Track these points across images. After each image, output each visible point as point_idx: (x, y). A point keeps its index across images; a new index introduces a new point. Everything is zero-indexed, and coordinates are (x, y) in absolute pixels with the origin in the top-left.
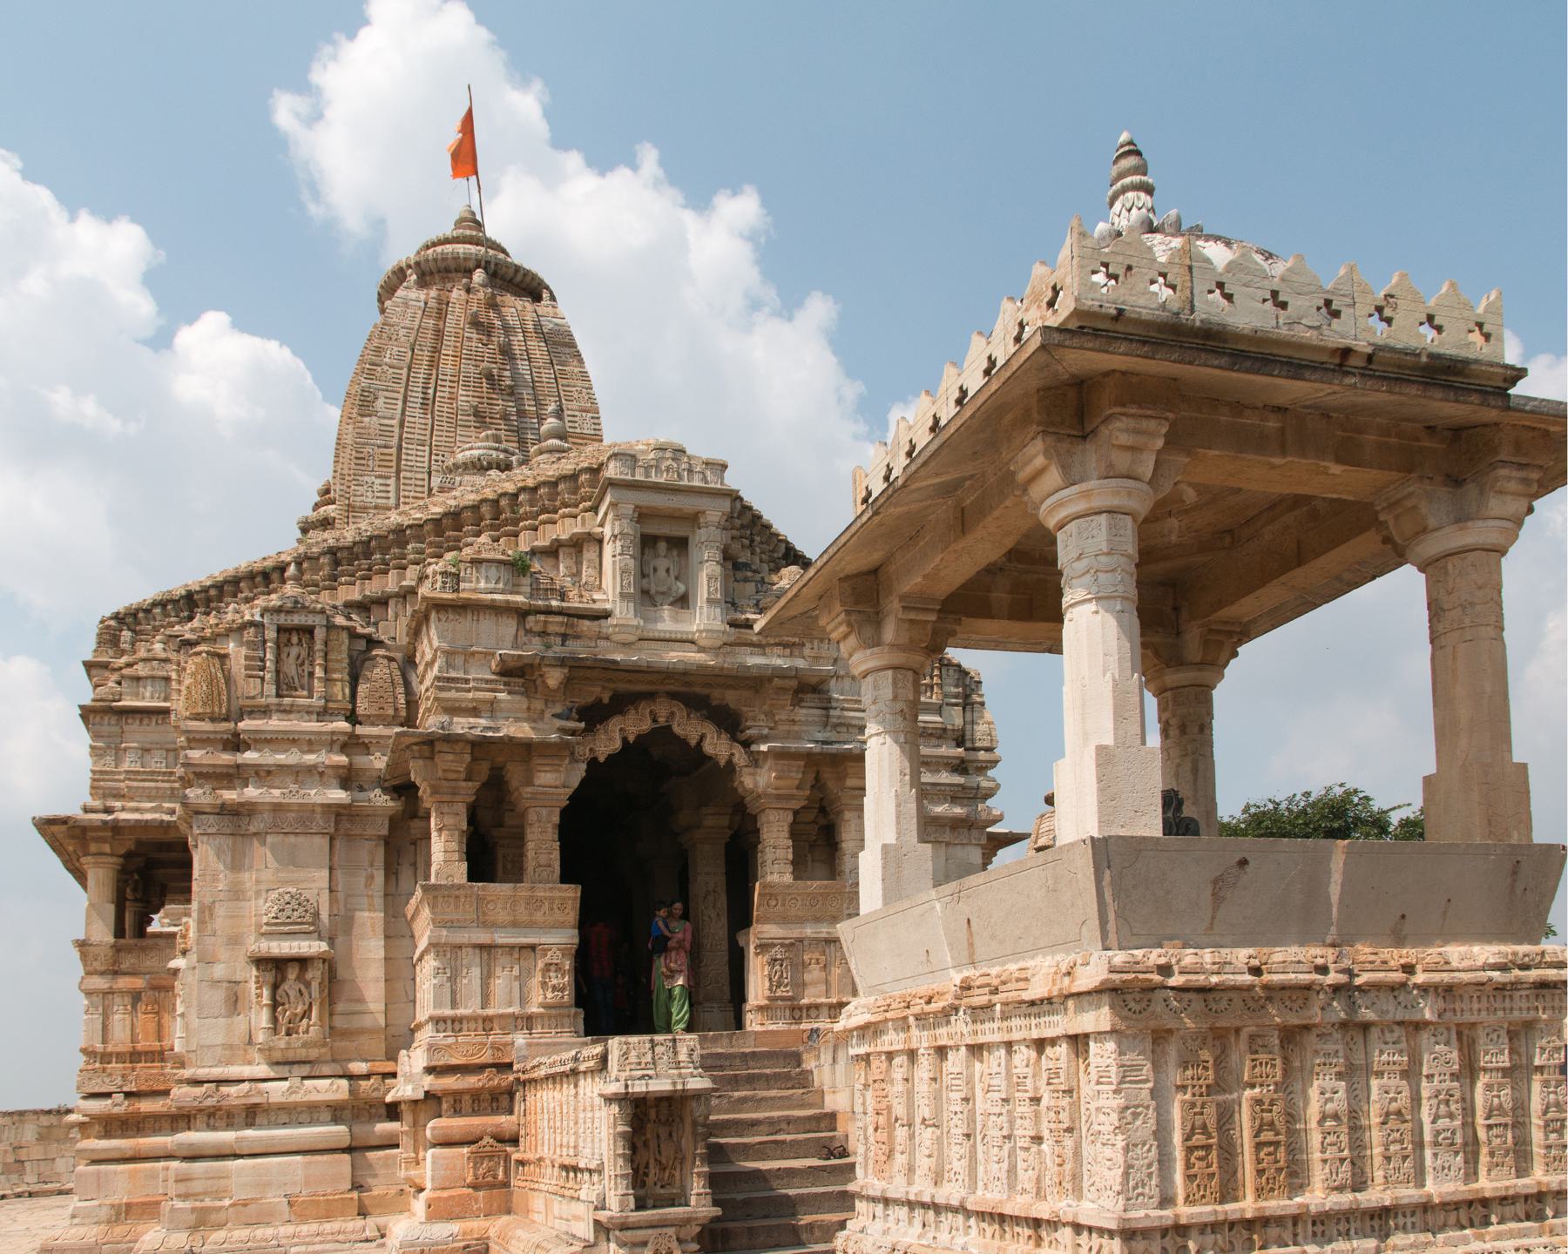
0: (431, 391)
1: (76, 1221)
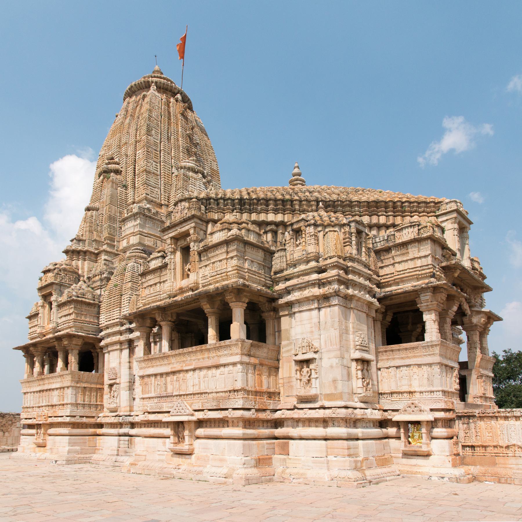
0: (170, 134)
1: (245, 466)
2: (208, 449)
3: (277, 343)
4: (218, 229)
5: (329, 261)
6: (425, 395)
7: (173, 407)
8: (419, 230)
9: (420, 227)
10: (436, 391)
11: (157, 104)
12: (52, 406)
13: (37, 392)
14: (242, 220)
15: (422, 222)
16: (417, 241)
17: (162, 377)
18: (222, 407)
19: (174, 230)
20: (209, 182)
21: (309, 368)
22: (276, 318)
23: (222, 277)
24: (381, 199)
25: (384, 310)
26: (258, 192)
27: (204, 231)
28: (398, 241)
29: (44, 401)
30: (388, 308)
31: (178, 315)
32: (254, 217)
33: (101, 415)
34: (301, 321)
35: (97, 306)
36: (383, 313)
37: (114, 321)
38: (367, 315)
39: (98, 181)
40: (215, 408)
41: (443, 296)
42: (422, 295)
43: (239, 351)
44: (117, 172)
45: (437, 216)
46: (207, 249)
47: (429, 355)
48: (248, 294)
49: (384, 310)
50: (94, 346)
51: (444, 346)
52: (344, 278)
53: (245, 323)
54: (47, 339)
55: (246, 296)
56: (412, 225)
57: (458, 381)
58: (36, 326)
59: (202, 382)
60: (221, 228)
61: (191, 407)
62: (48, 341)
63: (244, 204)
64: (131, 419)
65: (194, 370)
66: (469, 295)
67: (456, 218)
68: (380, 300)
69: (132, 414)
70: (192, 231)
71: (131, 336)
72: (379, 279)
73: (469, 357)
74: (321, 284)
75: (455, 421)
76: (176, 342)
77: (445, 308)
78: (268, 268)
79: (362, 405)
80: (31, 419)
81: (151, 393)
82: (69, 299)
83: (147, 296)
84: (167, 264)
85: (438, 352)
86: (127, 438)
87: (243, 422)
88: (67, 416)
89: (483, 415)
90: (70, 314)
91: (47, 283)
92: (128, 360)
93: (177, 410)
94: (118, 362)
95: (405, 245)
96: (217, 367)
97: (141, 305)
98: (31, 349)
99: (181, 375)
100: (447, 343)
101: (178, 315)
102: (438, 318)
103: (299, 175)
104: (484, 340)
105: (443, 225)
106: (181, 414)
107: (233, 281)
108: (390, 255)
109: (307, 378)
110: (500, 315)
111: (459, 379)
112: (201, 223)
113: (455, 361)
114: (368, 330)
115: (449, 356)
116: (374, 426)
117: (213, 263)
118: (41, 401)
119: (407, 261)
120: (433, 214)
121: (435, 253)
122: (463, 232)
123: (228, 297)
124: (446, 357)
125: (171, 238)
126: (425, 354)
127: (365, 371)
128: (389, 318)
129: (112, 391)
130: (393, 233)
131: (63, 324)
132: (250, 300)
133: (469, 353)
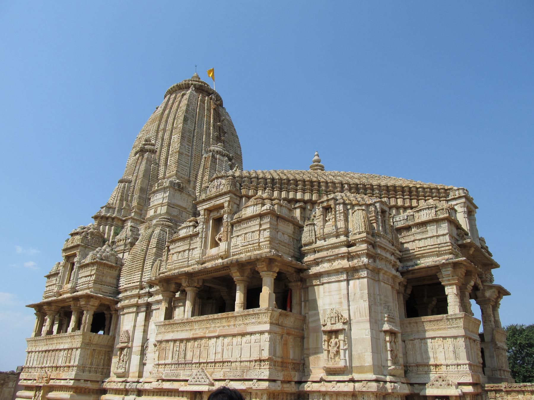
3: (303, 313)
5: (358, 236)
6: (451, 368)
8: (436, 211)
9: (437, 210)
10: (463, 365)
11: (194, 100)
12: (57, 367)
13: (42, 351)
16: (436, 221)
17: (182, 343)
18: (245, 378)
21: (338, 338)
23: (253, 247)
27: (238, 205)
28: (417, 221)
29: (49, 362)
30: (409, 281)
33: (107, 380)
34: (329, 292)
38: (392, 287)
40: (238, 378)
41: (462, 271)
42: (444, 270)
43: (268, 319)
44: (153, 152)
46: (240, 221)
48: (279, 264)
49: (405, 283)
50: (108, 308)
54: (64, 298)
55: (277, 266)
58: (54, 285)
59: (225, 350)
60: (255, 203)
61: (211, 375)
62: (64, 300)
63: (273, 184)
64: (139, 386)
65: (217, 337)
67: (464, 203)
68: (402, 274)
69: (141, 380)
70: (226, 205)
71: (150, 300)
74: (350, 257)
77: (464, 283)
78: (297, 240)
83: (175, 262)
84: (199, 233)
85: (462, 325)
87: (267, 394)
89: (510, 389)
90: (91, 276)
91: (72, 245)
93: (196, 379)
94: (133, 325)
95: (424, 224)
96: (243, 335)
99: (203, 341)
101: (204, 281)
102: (459, 292)
103: (319, 161)
106: (200, 383)
107: (265, 251)
108: (410, 233)
109: (336, 349)
110: (508, 290)
112: (236, 197)
115: (471, 329)
117: (246, 234)
118: (45, 362)
119: (426, 238)
123: (261, 267)
125: (205, 210)
126: (449, 326)
127: (393, 343)
128: (409, 292)
129: (122, 355)
130: (412, 213)
131: (83, 285)
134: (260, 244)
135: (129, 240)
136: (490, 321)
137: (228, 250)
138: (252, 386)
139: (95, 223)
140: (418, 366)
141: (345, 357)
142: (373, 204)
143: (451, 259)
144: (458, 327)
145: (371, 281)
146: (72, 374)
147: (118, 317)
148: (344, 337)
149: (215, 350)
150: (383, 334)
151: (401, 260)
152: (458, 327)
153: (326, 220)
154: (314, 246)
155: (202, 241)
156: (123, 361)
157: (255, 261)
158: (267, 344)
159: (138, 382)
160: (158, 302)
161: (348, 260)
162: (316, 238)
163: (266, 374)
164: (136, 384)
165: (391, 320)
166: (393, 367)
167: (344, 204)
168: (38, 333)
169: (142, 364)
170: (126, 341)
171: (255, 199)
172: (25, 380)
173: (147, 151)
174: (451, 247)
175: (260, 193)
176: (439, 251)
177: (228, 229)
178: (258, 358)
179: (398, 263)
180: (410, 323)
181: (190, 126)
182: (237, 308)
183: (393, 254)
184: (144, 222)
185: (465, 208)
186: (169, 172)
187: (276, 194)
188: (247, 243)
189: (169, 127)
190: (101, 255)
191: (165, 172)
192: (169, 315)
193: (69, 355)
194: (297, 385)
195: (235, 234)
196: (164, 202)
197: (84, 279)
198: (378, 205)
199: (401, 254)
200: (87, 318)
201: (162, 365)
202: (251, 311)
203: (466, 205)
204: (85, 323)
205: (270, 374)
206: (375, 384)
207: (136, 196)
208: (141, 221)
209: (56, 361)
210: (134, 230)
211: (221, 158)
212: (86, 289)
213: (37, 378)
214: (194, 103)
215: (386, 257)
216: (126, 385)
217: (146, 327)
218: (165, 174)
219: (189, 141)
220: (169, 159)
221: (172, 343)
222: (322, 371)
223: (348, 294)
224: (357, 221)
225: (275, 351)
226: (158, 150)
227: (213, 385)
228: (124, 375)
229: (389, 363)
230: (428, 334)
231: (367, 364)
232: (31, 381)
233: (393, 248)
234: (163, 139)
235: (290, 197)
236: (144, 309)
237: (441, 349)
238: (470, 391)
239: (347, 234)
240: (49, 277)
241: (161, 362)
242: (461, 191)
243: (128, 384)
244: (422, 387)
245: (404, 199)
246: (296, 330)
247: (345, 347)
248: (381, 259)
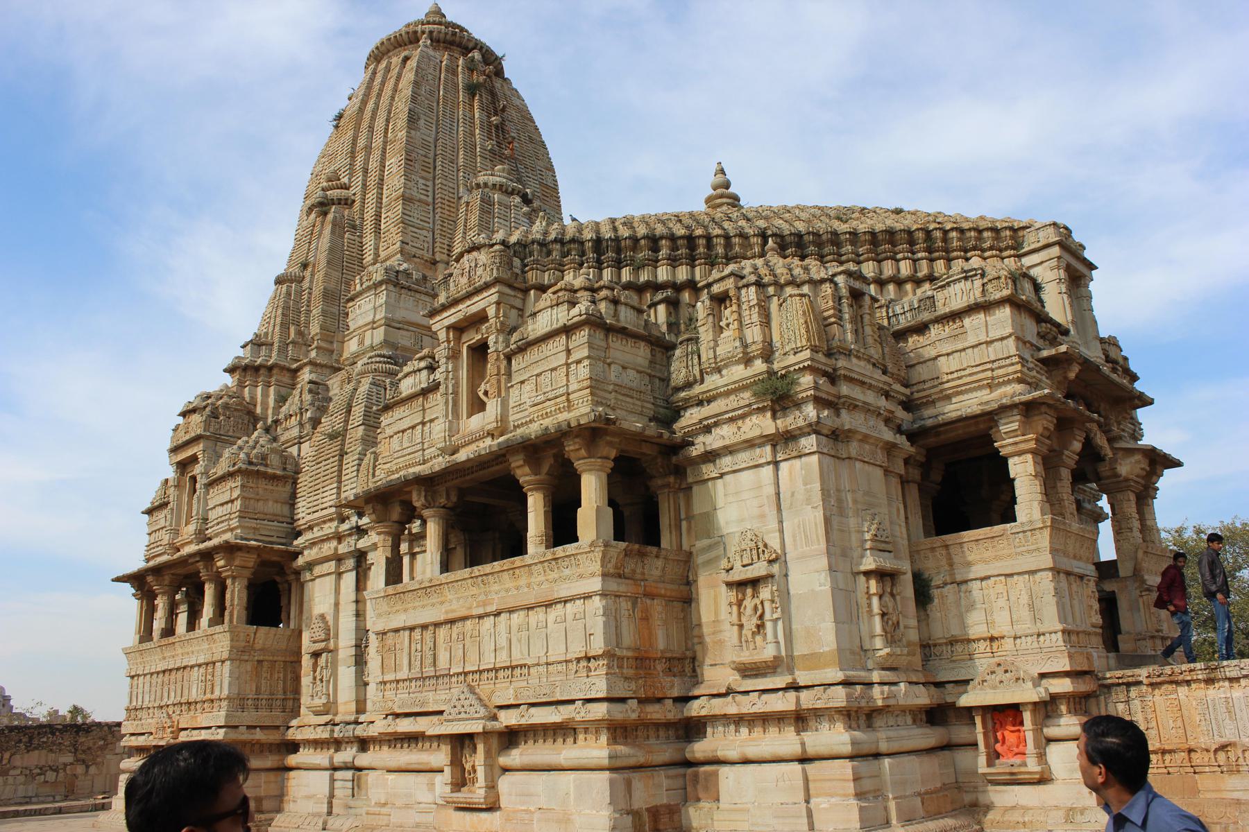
2: (531, 795)
3: (685, 547)
4: (548, 303)
5: (792, 359)
7: (450, 700)
11: (431, 71)
14: (601, 283)
15: (988, 270)
19: (453, 310)
20: (535, 211)
22: (680, 489)
24: (898, 226)
25: (923, 459)
26: (636, 225)
27: (520, 310)
28: (942, 310)
29: (172, 694)
30: (931, 453)
31: (462, 492)
32: (626, 275)
33: (294, 723)
35: (291, 481)
36: (921, 465)
37: (325, 512)
39: (305, 223)
41: (1044, 422)
43: (597, 567)
44: (347, 203)
45: (1020, 256)
47: (1028, 551)
48: (617, 440)
49: (923, 459)
51: (1060, 530)
52: (828, 393)
53: (611, 503)
54: (181, 557)
55: (610, 444)
56: (967, 276)
57: (1096, 606)
62: (184, 561)
64: (360, 731)
66: (1106, 418)
67: (1059, 258)
68: (912, 437)
69: (362, 718)
70: (491, 312)
71: (362, 544)
72: (907, 391)
73: (1118, 549)
75: (1097, 697)
76: (459, 555)
78: (662, 380)
79: (889, 676)
80: (143, 734)
81: (401, 670)
82: (231, 469)
83: (396, 455)
84: (439, 384)
86: (349, 774)
87: (608, 729)
88: (220, 727)
89: (1159, 680)
90: (232, 501)
91: (187, 437)
92: (353, 597)
93: (459, 707)
94: (333, 601)
96: (549, 605)
97: (383, 476)
98: (150, 579)
100: (1065, 524)
101: (462, 492)
102: (1040, 468)
104: (1146, 510)
105: (1033, 272)
107: (582, 411)
109: (755, 621)
110: (1175, 455)
111: (1100, 600)
112: (512, 293)
113: (1087, 561)
114: (889, 505)
116: (914, 721)
117: (537, 375)
118: (166, 695)
120: (1012, 252)
121: (1022, 330)
122: (1078, 286)
123: (572, 448)
124: (1065, 554)
125: (448, 328)
126: (1019, 550)
127: (887, 598)
128: (937, 476)
130: (930, 293)
132: (622, 451)
133: (1117, 541)
134: (571, 397)
135: (309, 414)
136: (1131, 529)
137: (503, 418)
138: (573, 715)
139: (229, 380)
140: (952, 642)
141: (776, 637)
142: (831, 280)
143: (1020, 394)
144: (1038, 549)
145: (827, 460)
146: (219, 716)
147: (302, 586)
148: (772, 593)
149: (493, 643)
150: (862, 578)
151: (908, 405)
152: (1038, 549)
153: (721, 328)
154: (697, 389)
155: (447, 402)
156: (321, 680)
157: (559, 439)
158: (600, 621)
159: (357, 723)
160: (374, 547)
161: (774, 417)
162: (701, 371)
163: (600, 687)
164: (352, 726)
165: (882, 545)
166: (887, 650)
167: (759, 284)
168: (146, 634)
169: (361, 684)
170: (323, 637)
171: (554, 293)
172: (132, 734)
173: (332, 202)
174: (1018, 367)
175: (569, 277)
176: (993, 378)
177: (499, 368)
178: (583, 655)
179: (900, 413)
180: (933, 549)
181: (425, 132)
182: (531, 548)
183: (887, 395)
184: (340, 369)
185: (1062, 271)
186: (385, 248)
187: (607, 274)
188: (542, 398)
189: (378, 142)
190: (248, 455)
191: (377, 249)
192: (394, 574)
193: (209, 677)
194: (678, 705)
195: (516, 378)
196: (378, 317)
197: (220, 511)
198: (840, 279)
199: (907, 391)
200: (236, 595)
201: (391, 682)
202: (560, 551)
203: (1063, 264)
204: (232, 605)
205: (609, 688)
206: (840, 691)
207: (316, 312)
208: (332, 367)
209: (186, 692)
210: (318, 388)
211: (504, 198)
212: (224, 532)
213: (153, 731)
214: (430, 77)
215: (864, 403)
216: (332, 731)
217: (361, 605)
218: (377, 255)
219: (425, 168)
220: (383, 216)
221: (407, 633)
222: (729, 671)
223: (778, 494)
224: (791, 327)
225: (618, 635)
226: (358, 198)
227: (494, 718)
228: (329, 708)
229: (878, 643)
230: (977, 571)
231: (826, 649)
232: (143, 738)
233: (885, 378)
234: (366, 171)
235: (642, 280)
236: (350, 563)
237: (1002, 602)
238: (1066, 690)
239: (768, 354)
240: (149, 512)
241: (388, 677)
242: (1051, 230)
243: (337, 728)
244: (961, 689)
245: (915, 261)
246: (669, 586)
247: (775, 616)
248: (853, 406)
